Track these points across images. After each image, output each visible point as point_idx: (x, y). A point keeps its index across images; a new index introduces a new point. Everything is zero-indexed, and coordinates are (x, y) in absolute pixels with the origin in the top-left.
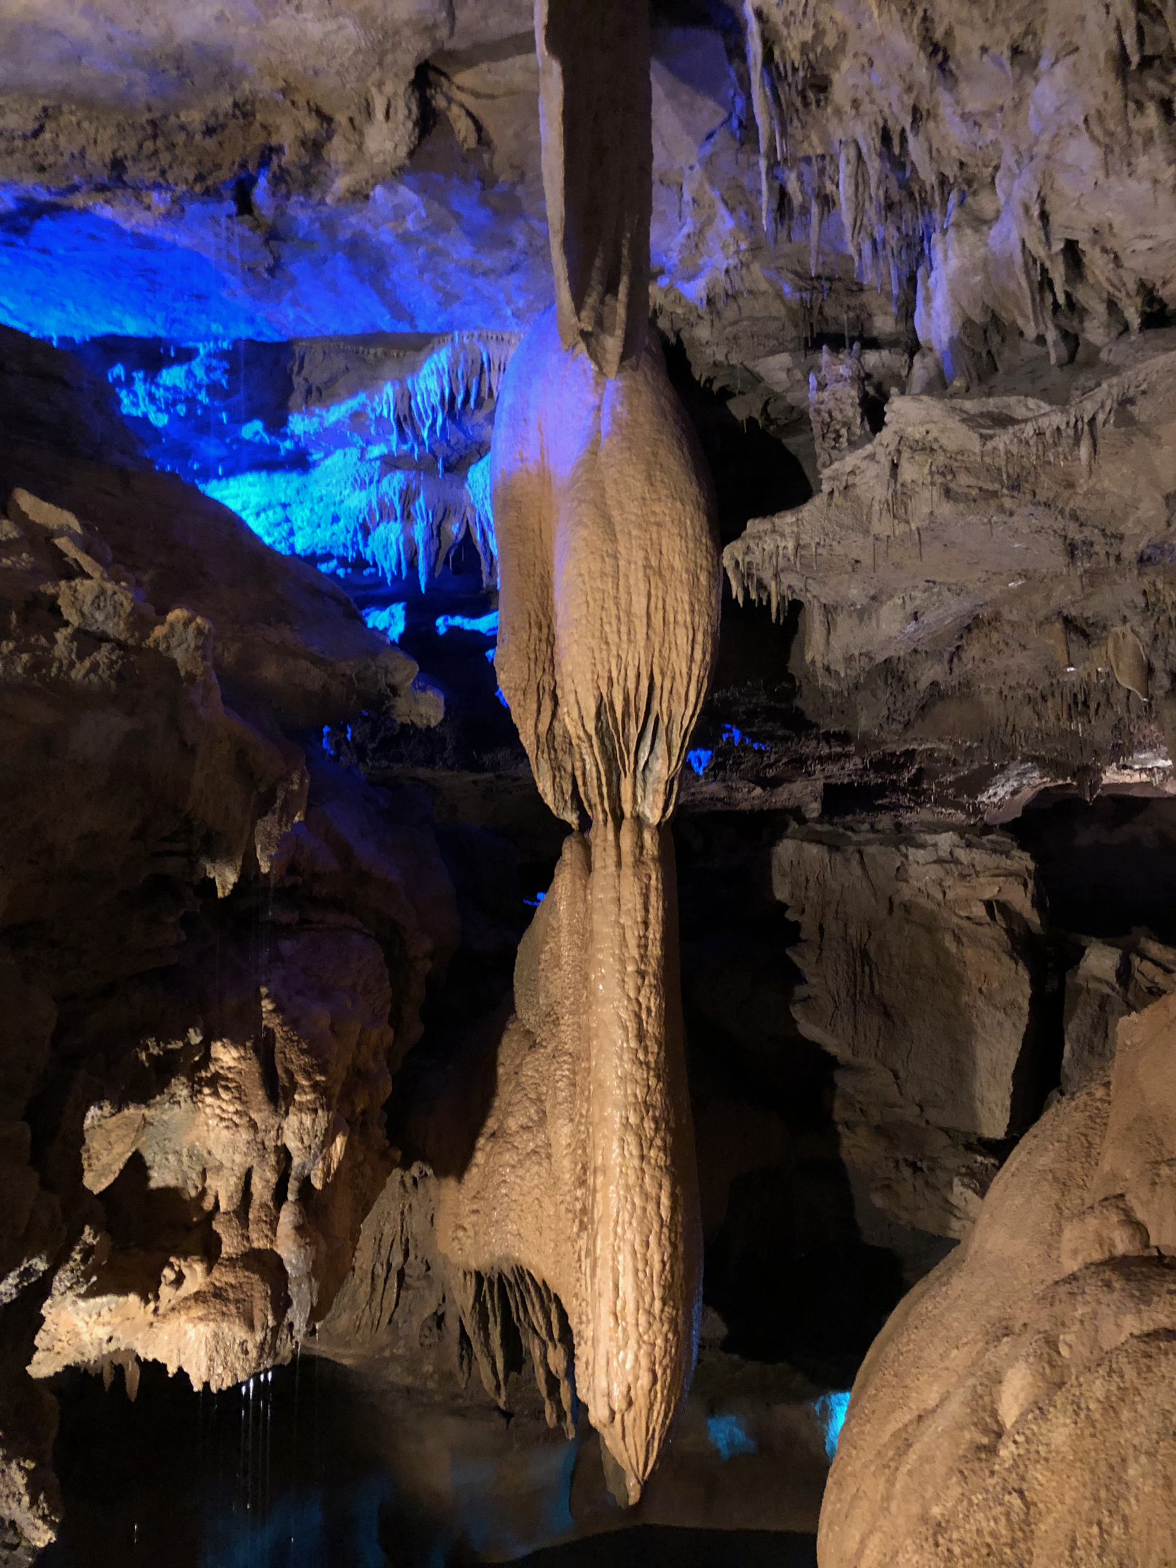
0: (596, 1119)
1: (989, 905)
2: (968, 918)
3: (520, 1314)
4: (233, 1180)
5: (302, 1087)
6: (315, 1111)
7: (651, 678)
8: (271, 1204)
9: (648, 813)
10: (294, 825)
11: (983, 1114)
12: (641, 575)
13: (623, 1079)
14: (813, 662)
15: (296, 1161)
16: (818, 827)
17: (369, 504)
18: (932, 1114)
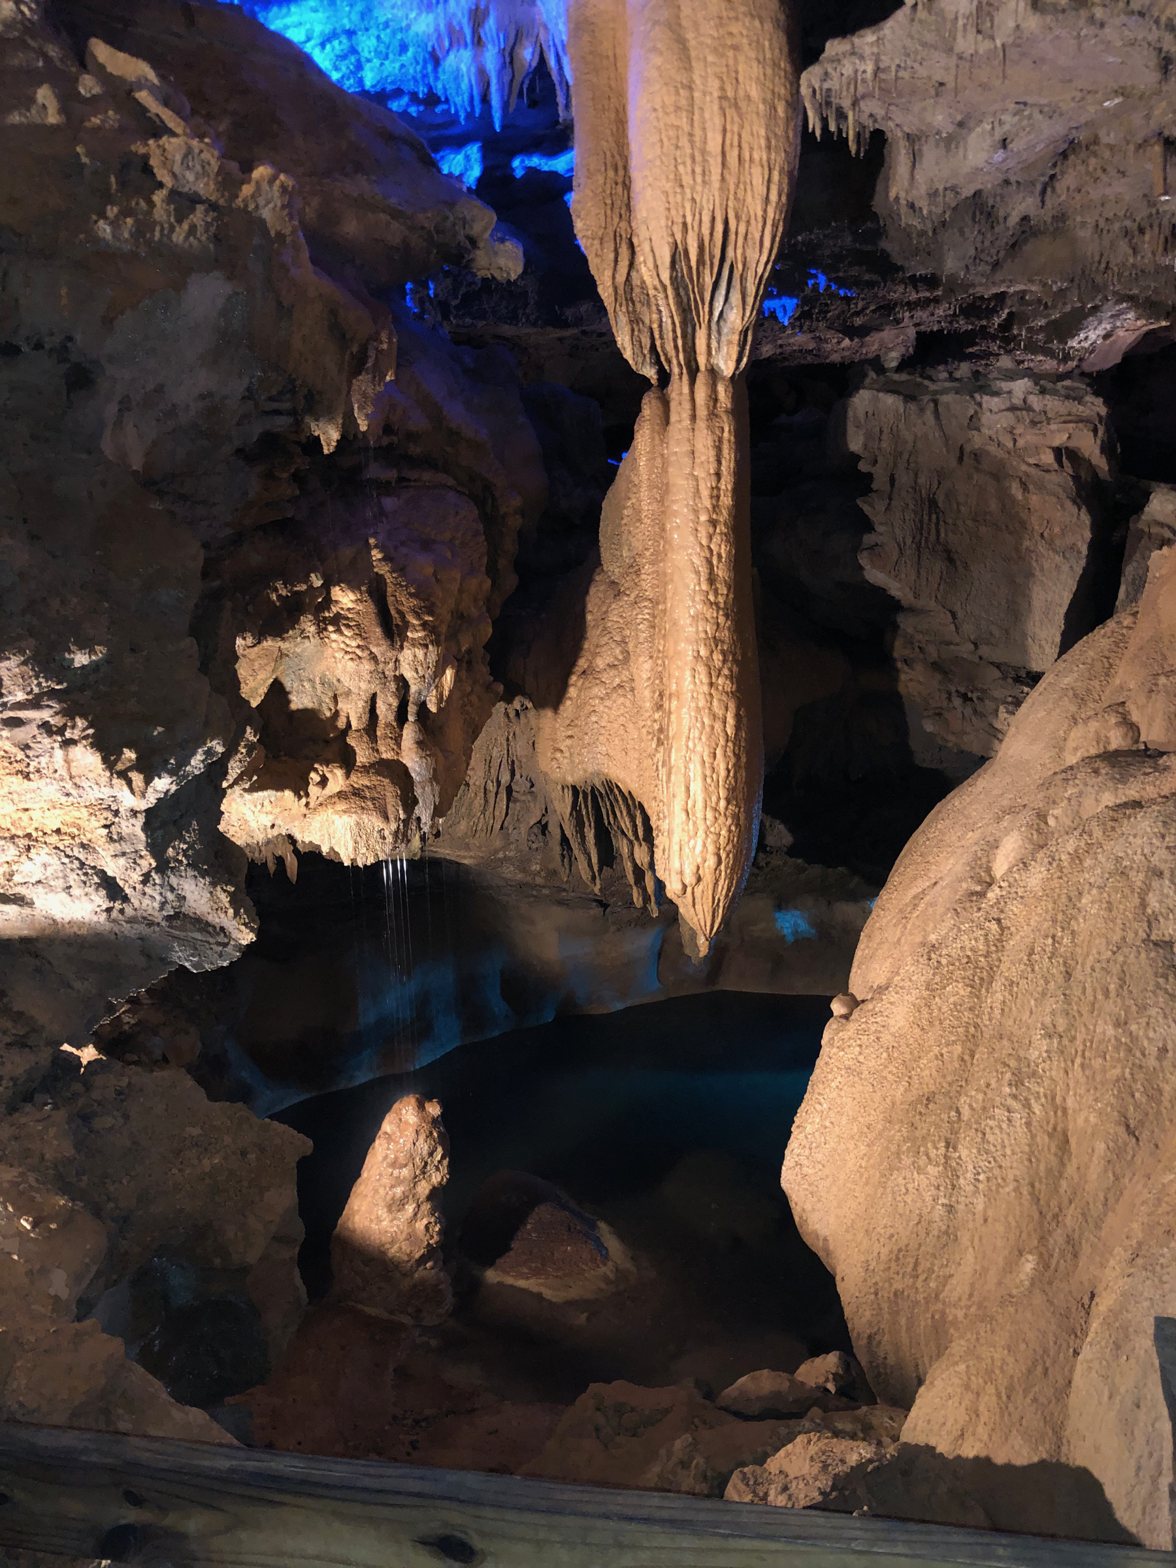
0: (671, 653)
1: (1058, 452)
2: (1037, 465)
3: (609, 817)
4: (361, 704)
5: (414, 625)
6: (426, 646)
7: (726, 223)
8: (395, 724)
9: (722, 366)
10: (386, 385)
11: (1034, 649)
12: (716, 107)
13: (695, 618)
14: (897, 198)
15: (413, 689)
16: (896, 377)
17: (437, 30)
18: (984, 650)
